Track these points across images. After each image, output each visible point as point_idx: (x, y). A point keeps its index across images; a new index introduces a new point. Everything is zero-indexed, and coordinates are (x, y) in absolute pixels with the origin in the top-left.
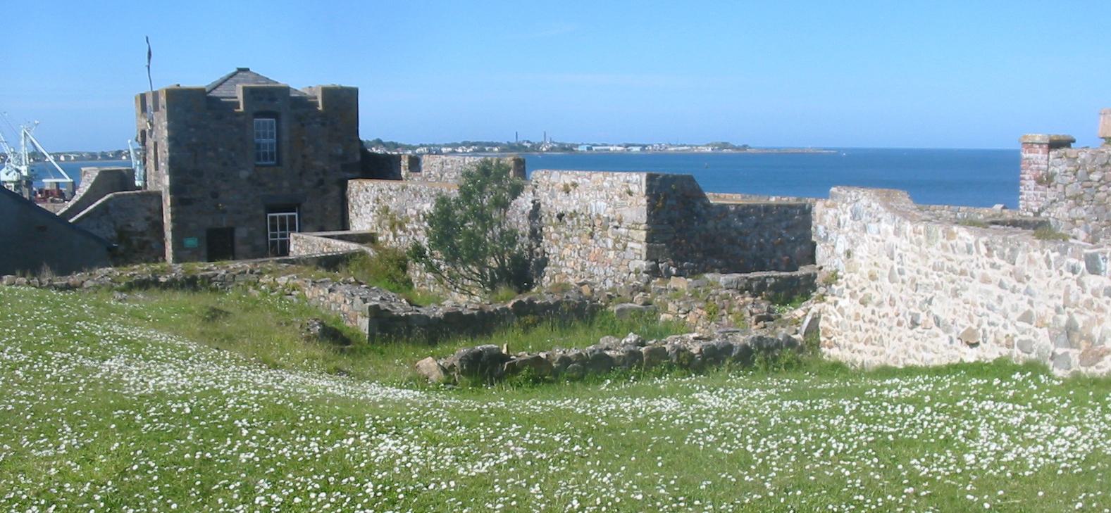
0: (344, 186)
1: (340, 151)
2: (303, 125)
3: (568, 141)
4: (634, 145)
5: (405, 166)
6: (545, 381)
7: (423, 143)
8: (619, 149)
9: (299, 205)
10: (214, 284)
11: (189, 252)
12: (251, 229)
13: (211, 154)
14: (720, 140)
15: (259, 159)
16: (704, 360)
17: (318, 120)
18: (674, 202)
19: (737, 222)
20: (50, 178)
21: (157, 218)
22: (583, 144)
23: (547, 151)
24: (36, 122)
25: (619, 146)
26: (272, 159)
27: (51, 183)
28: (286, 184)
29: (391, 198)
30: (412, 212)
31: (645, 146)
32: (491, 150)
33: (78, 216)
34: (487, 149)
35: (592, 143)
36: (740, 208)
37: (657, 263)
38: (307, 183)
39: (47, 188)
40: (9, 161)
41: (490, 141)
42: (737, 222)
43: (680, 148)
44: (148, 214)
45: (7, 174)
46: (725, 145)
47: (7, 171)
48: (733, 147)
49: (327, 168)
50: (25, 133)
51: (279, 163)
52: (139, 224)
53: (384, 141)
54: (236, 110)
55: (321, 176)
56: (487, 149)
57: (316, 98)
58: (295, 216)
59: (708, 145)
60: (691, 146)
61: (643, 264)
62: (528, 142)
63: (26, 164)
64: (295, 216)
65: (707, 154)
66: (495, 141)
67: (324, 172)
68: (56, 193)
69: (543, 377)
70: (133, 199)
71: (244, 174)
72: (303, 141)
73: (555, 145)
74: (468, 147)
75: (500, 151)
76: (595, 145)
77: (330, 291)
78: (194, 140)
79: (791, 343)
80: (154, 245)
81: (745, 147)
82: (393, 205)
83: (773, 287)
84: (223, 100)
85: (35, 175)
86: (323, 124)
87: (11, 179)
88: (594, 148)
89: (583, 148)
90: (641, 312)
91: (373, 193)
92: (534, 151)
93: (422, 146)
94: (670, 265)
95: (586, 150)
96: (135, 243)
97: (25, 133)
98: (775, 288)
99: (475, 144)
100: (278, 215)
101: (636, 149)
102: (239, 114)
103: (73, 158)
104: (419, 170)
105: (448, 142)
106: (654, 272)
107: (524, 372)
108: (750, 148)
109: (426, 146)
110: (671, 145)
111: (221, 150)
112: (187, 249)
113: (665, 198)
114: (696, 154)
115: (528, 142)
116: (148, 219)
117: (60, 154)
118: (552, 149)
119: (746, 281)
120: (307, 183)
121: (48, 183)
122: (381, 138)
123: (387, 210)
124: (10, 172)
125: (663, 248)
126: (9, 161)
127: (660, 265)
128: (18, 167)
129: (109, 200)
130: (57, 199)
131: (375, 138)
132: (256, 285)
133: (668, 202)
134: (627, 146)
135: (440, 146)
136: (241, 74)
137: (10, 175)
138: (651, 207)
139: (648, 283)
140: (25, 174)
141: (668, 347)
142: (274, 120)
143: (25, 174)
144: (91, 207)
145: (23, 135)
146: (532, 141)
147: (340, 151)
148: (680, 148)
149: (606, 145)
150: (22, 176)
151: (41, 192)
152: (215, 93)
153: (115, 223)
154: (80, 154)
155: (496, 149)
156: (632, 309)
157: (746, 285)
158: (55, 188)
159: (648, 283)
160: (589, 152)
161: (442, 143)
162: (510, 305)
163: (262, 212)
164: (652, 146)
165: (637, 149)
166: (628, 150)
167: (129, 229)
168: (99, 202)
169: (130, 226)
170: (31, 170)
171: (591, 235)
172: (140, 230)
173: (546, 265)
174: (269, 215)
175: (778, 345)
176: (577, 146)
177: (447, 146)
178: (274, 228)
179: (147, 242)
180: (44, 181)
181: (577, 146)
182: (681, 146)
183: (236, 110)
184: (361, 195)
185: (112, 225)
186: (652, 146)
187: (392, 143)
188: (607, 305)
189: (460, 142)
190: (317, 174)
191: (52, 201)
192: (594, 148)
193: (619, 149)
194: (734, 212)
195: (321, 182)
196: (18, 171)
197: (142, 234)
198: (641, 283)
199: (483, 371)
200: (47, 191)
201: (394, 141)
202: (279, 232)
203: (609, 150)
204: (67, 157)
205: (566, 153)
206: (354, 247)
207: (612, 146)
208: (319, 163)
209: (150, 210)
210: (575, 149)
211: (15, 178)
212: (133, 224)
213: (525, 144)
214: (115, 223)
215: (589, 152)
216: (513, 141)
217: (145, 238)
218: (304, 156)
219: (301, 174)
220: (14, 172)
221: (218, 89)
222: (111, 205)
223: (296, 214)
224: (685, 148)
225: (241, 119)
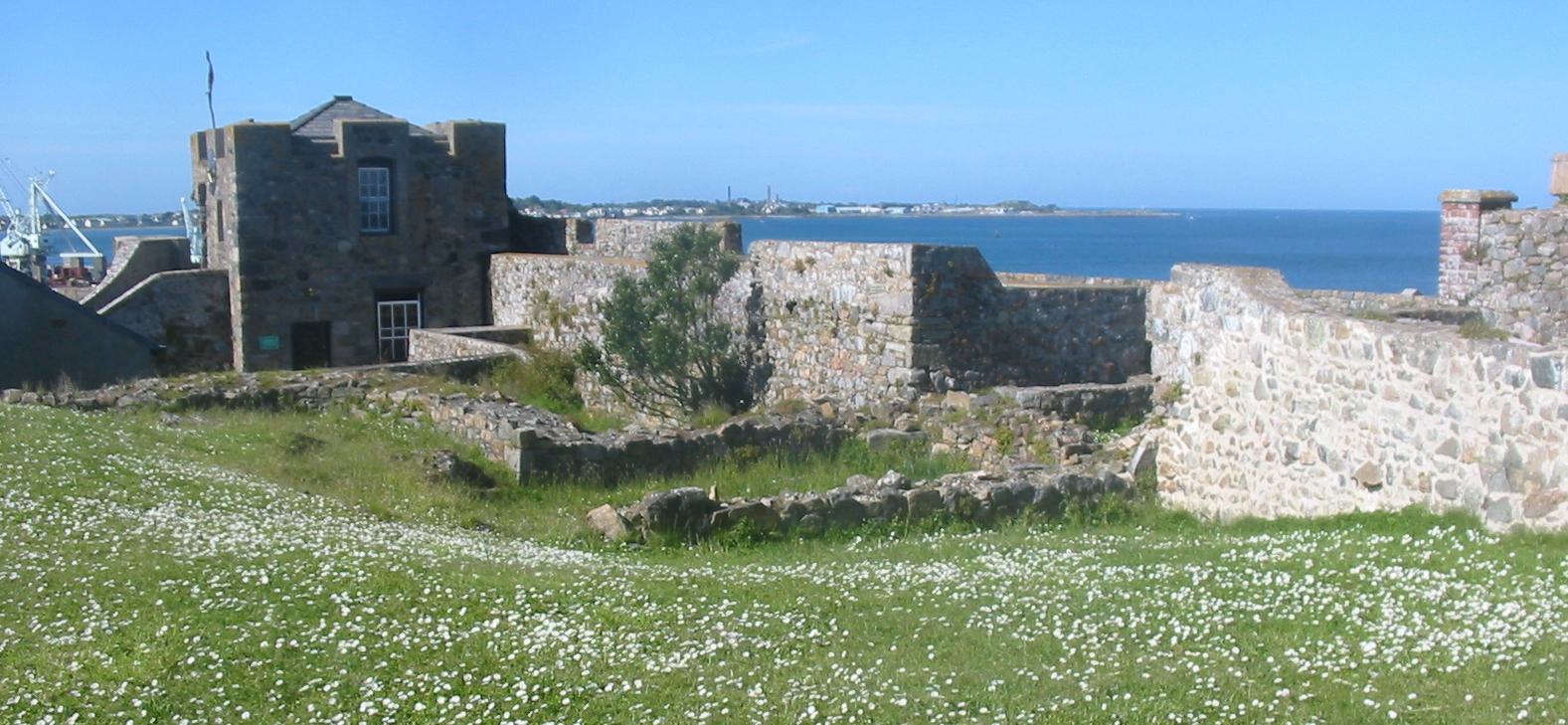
0: (485, 263)
1: (480, 214)
2: (427, 177)
3: (802, 199)
4: (895, 205)
5: (571, 235)
6: (769, 538)
7: (598, 203)
8: (874, 210)
9: (422, 290)
10: (302, 402)
11: (267, 356)
12: (355, 323)
13: (297, 217)
14: (1016, 198)
15: (365, 225)
16: (993, 509)
17: (449, 169)
18: (951, 286)
19: (1040, 314)
20: (71, 251)
21: (221, 308)
22: (822, 204)
23: (773, 213)
24: (51, 172)
25: (874, 206)
26: (384, 225)
27: (72, 258)
28: (403, 260)
29: (551, 280)
30: (581, 299)
31: (910, 206)
32: (693, 213)
33: (110, 305)
34: (687, 210)
35: (835, 202)
36: (1044, 293)
37: (928, 372)
38: (433, 259)
39: (67, 265)
40: (13, 227)
41: (691, 199)
42: (1040, 314)
43: (960, 210)
44: (209, 302)
45: (10, 246)
46: (1023, 205)
47: (10, 242)
48: (1035, 208)
49: (462, 237)
50: (35, 189)
51: (394, 231)
52: (196, 317)
53: (542, 199)
54: (333, 156)
55: (453, 249)
56: (687, 210)
57: (446, 138)
58: (416, 305)
59: (999, 205)
60: (975, 206)
61: (908, 373)
62: (745, 200)
63: (37, 232)
64: (416, 305)
65: (999, 217)
66: (698, 200)
67: (458, 243)
68: (79, 272)
69: (766, 533)
70: (188, 282)
71: (344, 246)
72: (428, 199)
73: (784, 205)
74: (661, 208)
75: (705, 214)
76: (840, 205)
77: (466, 411)
78: (273, 198)
79: (1117, 485)
80: (217, 347)
81: (1051, 207)
82: (554, 290)
83: (1092, 406)
84: (314, 141)
85: (49, 248)
86: (456, 176)
87: (15, 253)
88: (838, 209)
89: (822, 210)
90: (904, 440)
91: (527, 273)
92: (754, 213)
93: (595, 206)
94: (945, 375)
95: (826, 211)
96: (191, 343)
97: (35, 189)
98: (1094, 406)
99: (670, 204)
100: (392, 303)
101: (898, 211)
102: (337, 161)
103: (102, 223)
104: (592, 241)
105: (632, 201)
106: (923, 385)
107: (740, 526)
108: (1058, 209)
109: (601, 206)
110: (947, 206)
111: (312, 211)
112: (264, 352)
113: (938, 280)
114: (982, 217)
115: (745, 200)
116: (208, 309)
117: (85, 217)
118: (780, 211)
119: (1053, 396)
120: (433, 259)
121: (68, 258)
122: (538, 195)
123: (546, 296)
124: (14, 243)
125: (936, 350)
126: (13, 227)
127: (932, 375)
128: (25, 236)
129: (154, 282)
130: (81, 281)
131: (529, 196)
132: (361, 403)
133: (943, 286)
134: (885, 206)
135: (621, 207)
136: (340, 104)
137: (15, 247)
138: (919, 292)
139: (915, 400)
140: (35, 245)
141: (943, 491)
142: (386, 169)
143: (35, 245)
144: (129, 293)
145: (32, 191)
146: (751, 199)
147: (480, 214)
148: (960, 210)
149: (855, 205)
150: (31, 249)
151: (57, 271)
152: (304, 132)
153: (162, 315)
154: (113, 217)
155: (700, 211)
156: (891, 437)
157: (1053, 402)
158: (77, 265)
159: (915, 400)
160: (832, 215)
161: (624, 202)
162: (719, 432)
163: (369, 299)
164: (921, 206)
165: (899, 211)
166: (887, 212)
167: (182, 324)
168: (140, 285)
169: (183, 319)
170: (43, 240)
171: (835, 333)
172: (197, 325)
173: (770, 375)
174: (380, 304)
175: (1098, 487)
176: (815, 206)
177: (630, 206)
178: (386, 322)
179: (208, 342)
180: (62, 255)
181: (815, 206)
182: (961, 206)
183: (333, 156)
184: (509, 275)
185: (158, 318)
186: (921, 206)
187: (554, 202)
188: (856, 431)
189: (649, 201)
190: (447, 246)
191: (74, 284)
192: (838, 209)
193: (874, 210)
194: (1037, 300)
195: (453, 257)
196: (25, 241)
197: (201, 330)
198: (905, 400)
199: (681, 524)
200: (66, 270)
201: (557, 199)
202: (393, 328)
203: (859, 212)
204: (95, 223)
205: (799, 216)
206: (499, 349)
207: (864, 206)
208: (450, 231)
209: (211, 296)
210: (811, 210)
211: (21, 252)
212: (187, 317)
213: (741, 204)
214: (162, 315)
215: (832, 215)
216: (724, 199)
217: (205, 337)
218: (429, 221)
219: (424, 246)
220: (20, 242)
221: (308, 126)
222: (157, 290)
223: (418, 303)
224: (967, 209)
225: (340, 168)
